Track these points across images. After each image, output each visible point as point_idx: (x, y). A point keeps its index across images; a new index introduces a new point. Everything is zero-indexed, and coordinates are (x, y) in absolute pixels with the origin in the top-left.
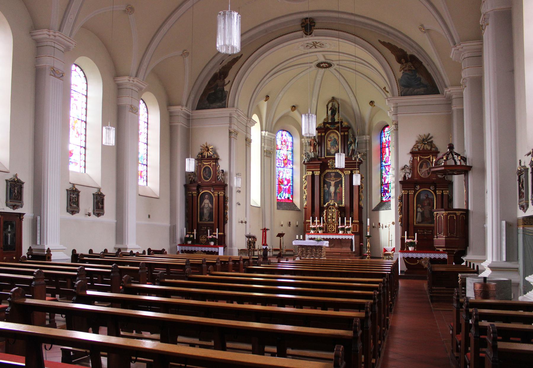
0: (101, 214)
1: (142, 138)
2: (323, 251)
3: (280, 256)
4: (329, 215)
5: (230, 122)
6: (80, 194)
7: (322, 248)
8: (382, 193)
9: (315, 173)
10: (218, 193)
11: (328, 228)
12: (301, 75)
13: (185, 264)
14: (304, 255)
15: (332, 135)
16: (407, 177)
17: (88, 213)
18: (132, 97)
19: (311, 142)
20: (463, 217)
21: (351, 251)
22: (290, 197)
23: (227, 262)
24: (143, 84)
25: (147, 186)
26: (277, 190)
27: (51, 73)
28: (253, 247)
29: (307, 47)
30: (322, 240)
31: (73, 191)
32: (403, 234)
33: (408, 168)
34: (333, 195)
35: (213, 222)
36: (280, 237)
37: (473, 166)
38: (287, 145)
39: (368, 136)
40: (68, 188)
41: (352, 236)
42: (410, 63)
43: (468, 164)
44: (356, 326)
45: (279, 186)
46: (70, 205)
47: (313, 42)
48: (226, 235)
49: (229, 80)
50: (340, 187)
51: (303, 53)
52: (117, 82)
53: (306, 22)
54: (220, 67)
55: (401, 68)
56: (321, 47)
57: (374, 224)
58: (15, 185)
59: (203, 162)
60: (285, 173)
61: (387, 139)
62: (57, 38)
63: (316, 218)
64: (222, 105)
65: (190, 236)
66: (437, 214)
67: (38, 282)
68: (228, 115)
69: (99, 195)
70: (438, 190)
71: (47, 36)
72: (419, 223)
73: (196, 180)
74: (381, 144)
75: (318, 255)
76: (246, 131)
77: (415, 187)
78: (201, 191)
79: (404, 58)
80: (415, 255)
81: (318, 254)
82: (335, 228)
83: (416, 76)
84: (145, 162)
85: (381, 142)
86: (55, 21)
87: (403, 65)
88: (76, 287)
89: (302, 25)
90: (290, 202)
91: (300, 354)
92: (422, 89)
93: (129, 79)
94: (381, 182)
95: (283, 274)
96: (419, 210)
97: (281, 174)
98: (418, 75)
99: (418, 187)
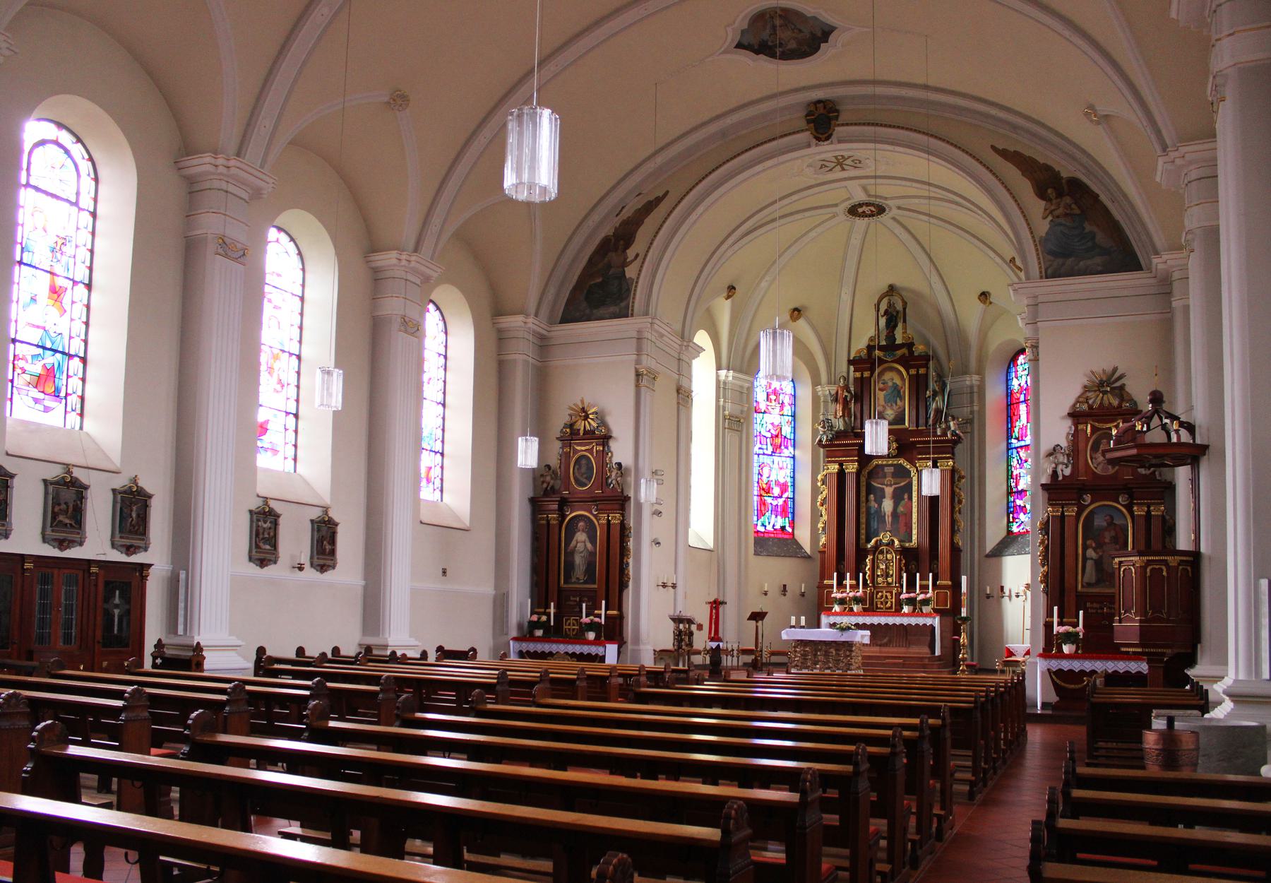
0: (329, 566)
1: (431, 391)
2: (853, 654)
3: (756, 666)
4: (878, 567)
5: (638, 352)
6: (281, 521)
7: (852, 647)
8: (1011, 513)
9: (847, 468)
10: (608, 516)
11: (877, 598)
12: (813, 234)
13: (495, 681)
14: (809, 664)
15: (888, 376)
16: (1060, 473)
17: (299, 564)
18: (405, 298)
19: (837, 392)
20: (1186, 569)
21: (929, 656)
22: (787, 525)
23: (607, 678)
24: (433, 267)
25: (442, 500)
26: (756, 508)
27: (217, 249)
28: (687, 645)
29: (821, 168)
30: (853, 627)
31: (264, 513)
32: (1050, 614)
33: (1062, 453)
34: (888, 519)
35: (595, 586)
36: (757, 622)
37: (1210, 444)
38: (781, 402)
39: (976, 377)
40: (253, 508)
41: (934, 618)
42: (1068, 197)
43: (1198, 441)
44: (728, 817)
45: (761, 499)
46: (257, 546)
47: (836, 157)
48: (625, 615)
49: (636, 252)
50: (906, 500)
51: (813, 182)
52: (373, 265)
53: (816, 110)
54: (617, 221)
55: (1046, 210)
56: (856, 167)
57: (988, 588)
58: (133, 500)
59: (575, 443)
60: (776, 469)
61: (1023, 384)
62: (233, 171)
63: (848, 574)
64: (620, 311)
65: (539, 619)
66: (1120, 562)
67: (132, 715)
68: (635, 334)
69: (324, 522)
70: (1137, 504)
71: (211, 168)
72: (1089, 585)
73: (557, 487)
74: (1007, 396)
75: (841, 665)
76: (679, 371)
77: (1080, 498)
78: (567, 513)
79: (1055, 188)
80: (1076, 665)
81: (843, 662)
82: (892, 598)
83: (1084, 229)
84: (438, 447)
85: (1007, 391)
86: (229, 135)
87: (1052, 205)
88: (189, 725)
89: (836, 114)
90: (786, 537)
91: (538, 869)
92: (1098, 260)
93: (398, 256)
94: (1009, 487)
95: (775, 710)
96: (1091, 553)
97: (766, 472)
98: (1088, 227)
99: (1088, 498)
